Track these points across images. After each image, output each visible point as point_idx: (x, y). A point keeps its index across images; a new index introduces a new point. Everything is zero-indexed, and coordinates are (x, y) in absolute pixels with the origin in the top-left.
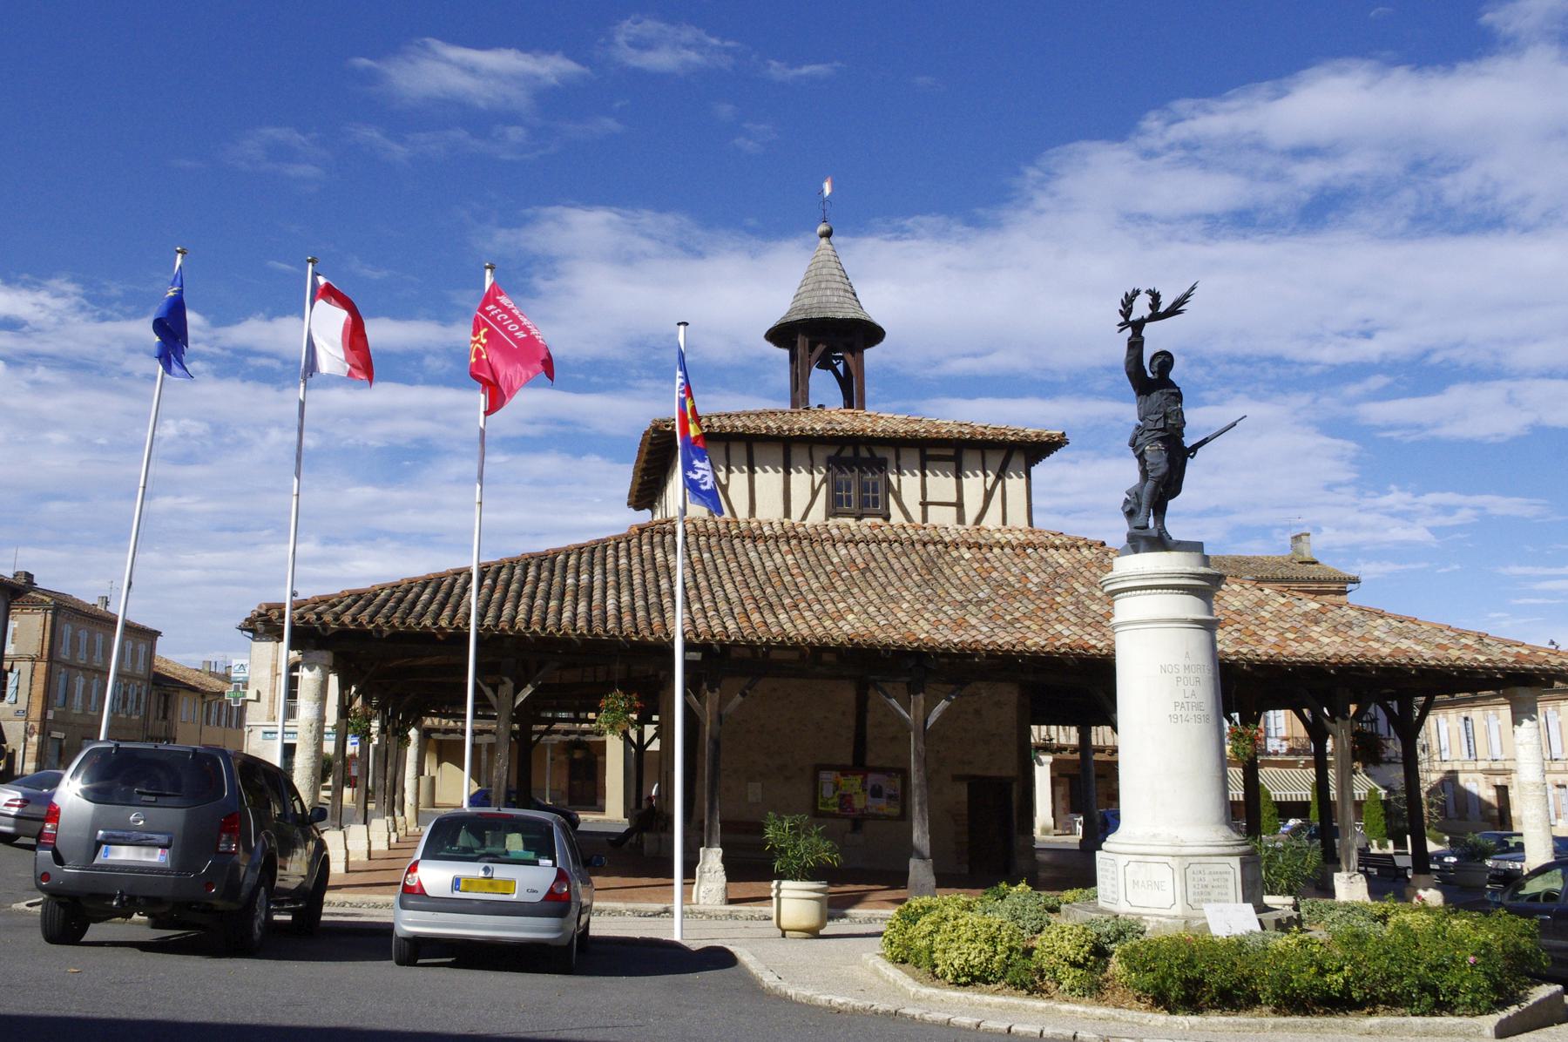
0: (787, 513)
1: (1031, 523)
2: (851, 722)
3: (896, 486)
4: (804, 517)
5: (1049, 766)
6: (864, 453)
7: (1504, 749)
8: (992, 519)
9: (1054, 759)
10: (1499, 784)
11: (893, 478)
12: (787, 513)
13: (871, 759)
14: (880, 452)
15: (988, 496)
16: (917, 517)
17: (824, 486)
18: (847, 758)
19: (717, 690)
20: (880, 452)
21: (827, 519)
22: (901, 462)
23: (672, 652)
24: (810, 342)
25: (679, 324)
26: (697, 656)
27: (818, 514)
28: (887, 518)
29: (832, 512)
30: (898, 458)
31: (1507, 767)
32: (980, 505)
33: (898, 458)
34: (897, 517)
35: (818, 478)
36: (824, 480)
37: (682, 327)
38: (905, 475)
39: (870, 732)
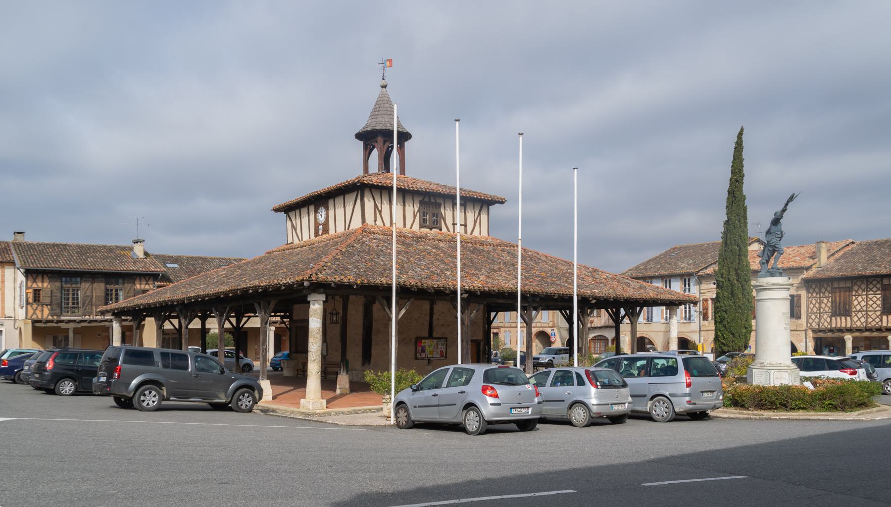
0: (405, 226)
1: (375, 224)
2: (428, 318)
3: (444, 216)
4: (411, 228)
5: (273, 332)
6: (433, 200)
7: (512, 317)
8: (476, 233)
9: (276, 328)
10: (495, 332)
11: (443, 211)
12: (405, 226)
13: (435, 335)
14: (438, 201)
15: (475, 222)
16: (451, 230)
17: (418, 213)
18: (426, 334)
19: (469, 308)
20: (438, 201)
21: (420, 229)
22: (446, 205)
23: (517, 296)
24: (384, 140)
25: (574, 169)
26: (466, 296)
27: (416, 227)
28: (441, 230)
29: (421, 227)
30: (444, 204)
31: (499, 325)
32: (473, 226)
33: (444, 204)
34: (444, 230)
35: (416, 209)
36: (419, 211)
37: (576, 170)
38: (384, 204)
39: (435, 323)
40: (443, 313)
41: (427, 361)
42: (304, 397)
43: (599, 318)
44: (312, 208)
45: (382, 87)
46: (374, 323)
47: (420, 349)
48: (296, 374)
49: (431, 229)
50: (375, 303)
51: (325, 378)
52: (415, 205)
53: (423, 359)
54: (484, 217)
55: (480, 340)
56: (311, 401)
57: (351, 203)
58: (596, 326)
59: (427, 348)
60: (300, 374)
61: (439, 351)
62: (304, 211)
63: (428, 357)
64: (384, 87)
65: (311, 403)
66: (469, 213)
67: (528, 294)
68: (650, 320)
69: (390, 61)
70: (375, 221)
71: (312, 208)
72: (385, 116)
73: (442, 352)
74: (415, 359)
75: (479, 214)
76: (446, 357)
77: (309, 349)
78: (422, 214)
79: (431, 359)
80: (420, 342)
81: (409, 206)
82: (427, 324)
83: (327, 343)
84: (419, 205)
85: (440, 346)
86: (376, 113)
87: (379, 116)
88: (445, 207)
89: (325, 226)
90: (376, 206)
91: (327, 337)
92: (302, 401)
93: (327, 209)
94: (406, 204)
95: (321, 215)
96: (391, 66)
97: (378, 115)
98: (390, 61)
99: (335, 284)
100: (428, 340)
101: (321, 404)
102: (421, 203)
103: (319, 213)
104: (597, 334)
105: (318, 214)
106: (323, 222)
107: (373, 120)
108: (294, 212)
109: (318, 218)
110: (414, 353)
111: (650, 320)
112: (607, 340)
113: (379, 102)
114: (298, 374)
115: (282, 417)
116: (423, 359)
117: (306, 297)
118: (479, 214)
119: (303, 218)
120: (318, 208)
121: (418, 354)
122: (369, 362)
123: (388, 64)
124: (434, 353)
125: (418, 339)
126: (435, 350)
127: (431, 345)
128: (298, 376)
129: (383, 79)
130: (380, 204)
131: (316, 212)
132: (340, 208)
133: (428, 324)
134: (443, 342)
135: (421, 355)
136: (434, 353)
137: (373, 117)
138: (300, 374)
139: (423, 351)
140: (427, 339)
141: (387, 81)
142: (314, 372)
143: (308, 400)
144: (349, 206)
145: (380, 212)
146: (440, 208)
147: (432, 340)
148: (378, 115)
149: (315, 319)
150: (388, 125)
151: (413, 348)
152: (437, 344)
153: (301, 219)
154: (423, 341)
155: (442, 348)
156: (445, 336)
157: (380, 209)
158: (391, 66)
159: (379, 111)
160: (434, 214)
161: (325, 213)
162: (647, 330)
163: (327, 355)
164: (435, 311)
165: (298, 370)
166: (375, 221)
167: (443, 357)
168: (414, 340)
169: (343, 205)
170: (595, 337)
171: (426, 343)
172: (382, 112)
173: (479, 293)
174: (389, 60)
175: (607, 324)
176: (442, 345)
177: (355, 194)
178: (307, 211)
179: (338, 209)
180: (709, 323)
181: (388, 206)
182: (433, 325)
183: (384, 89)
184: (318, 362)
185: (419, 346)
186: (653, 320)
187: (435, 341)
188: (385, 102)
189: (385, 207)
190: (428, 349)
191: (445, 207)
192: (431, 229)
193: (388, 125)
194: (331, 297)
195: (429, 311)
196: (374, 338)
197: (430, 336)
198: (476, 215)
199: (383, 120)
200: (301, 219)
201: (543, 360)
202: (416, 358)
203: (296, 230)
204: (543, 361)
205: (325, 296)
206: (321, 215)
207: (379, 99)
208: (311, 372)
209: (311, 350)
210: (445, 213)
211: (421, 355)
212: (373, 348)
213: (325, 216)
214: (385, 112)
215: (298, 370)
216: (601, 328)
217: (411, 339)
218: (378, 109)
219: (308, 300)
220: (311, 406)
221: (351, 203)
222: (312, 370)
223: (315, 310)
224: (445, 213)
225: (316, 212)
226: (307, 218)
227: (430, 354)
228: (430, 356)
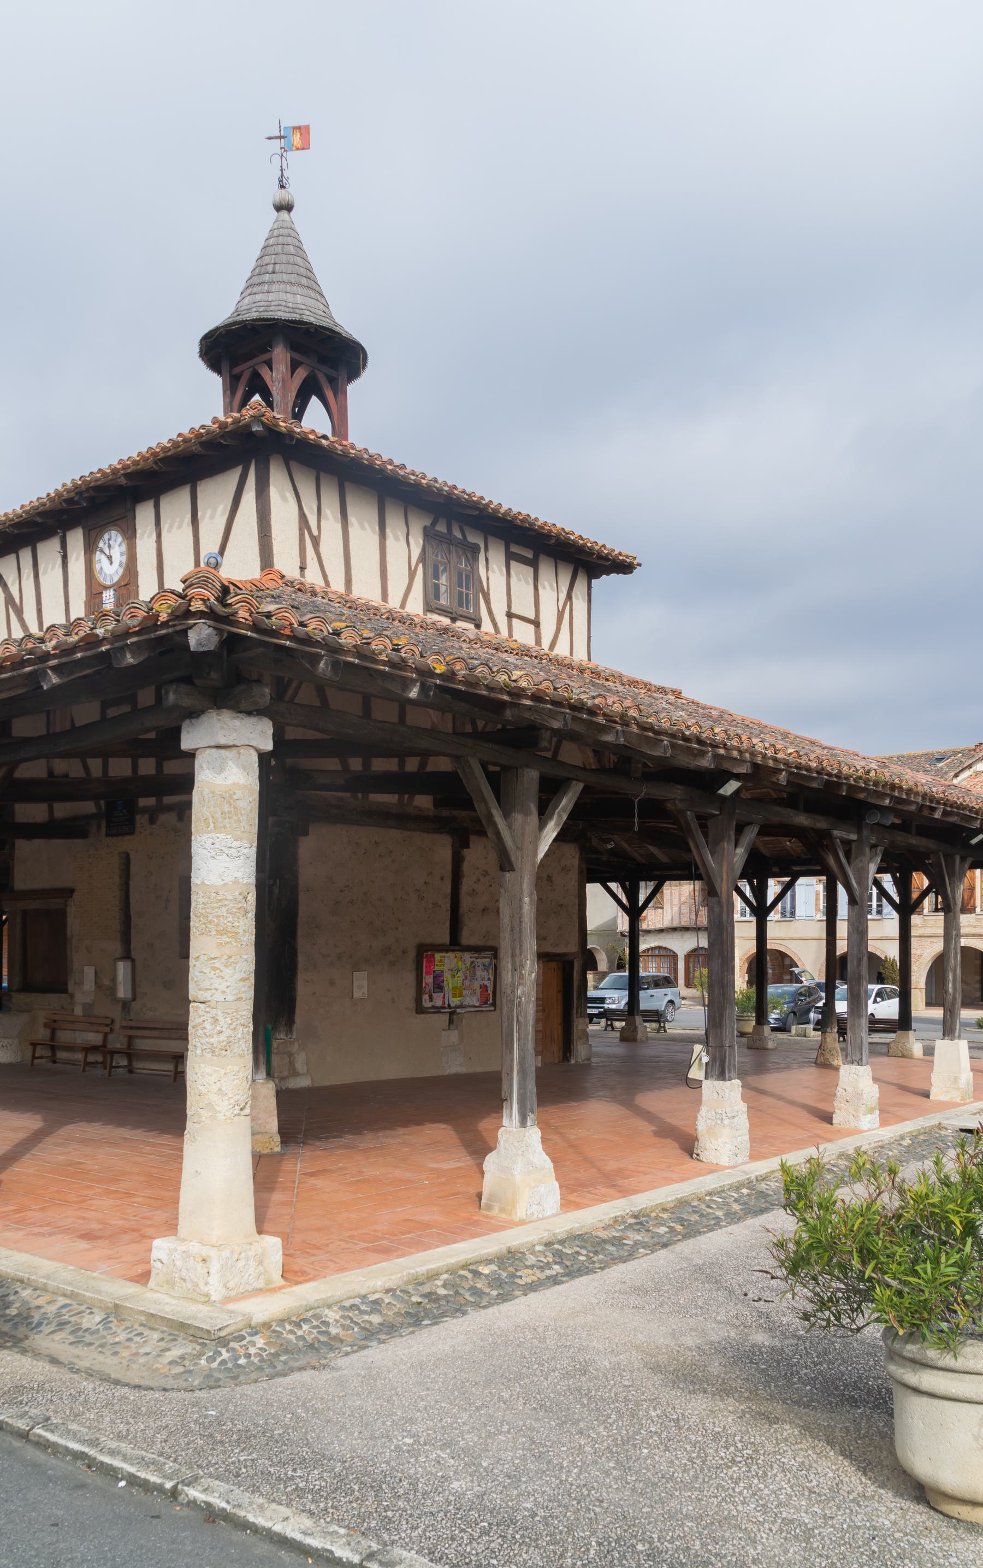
0: (385, 596)
2: (448, 888)
12: (385, 596)
13: (466, 939)
17: (421, 566)
28: (478, 626)
29: (429, 608)
30: (486, 550)
33: (486, 550)
34: (487, 626)
35: (416, 551)
36: (423, 558)
39: (466, 902)
40: (486, 874)
41: (446, 1017)
42: (171, 1227)
43: (659, 910)
44: (76, 539)
45: (279, 208)
46: (303, 899)
47: (428, 980)
48: (29, 1055)
49: (454, 620)
50: (306, 834)
51: (131, 1071)
52: (411, 540)
53: (437, 1010)
54: (579, 604)
55: (571, 954)
56: (213, 1253)
57: (220, 508)
58: (651, 927)
59: (447, 976)
60: (41, 1057)
61: (477, 985)
62: (49, 550)
63: (449, 1005)
64: (288, 207)
65: (215, 1267)
66: (544, 588)
67: (884, 795)
68: (788, 914)
69: (303, 131)
70: (302, 569)
71: (76, 539)
72: (295, 289)
73: (484, 988)
74: (417, 1013)
75: (569, 597)
76: (494, 1004)
77: (193, 992)
78: (430, 571)
79: (458, 1011)
80: (431, 960)
81: (397, 539)
82: (446, 905)
83: (133, 961)
84: (421, 542)
85: (479, 973)
86: (267, 278)
87: (275, 287)
88: (487, 560)
89: (124, 591)
90: (302, 516)
91: (133, 944)
92: (161, 1247)
93: (130, 535)
94: (388, 531)
95: (110, 558)
96: (305, 146)
97: (271, 283)
98: (303, 131)
99: (335, 665)
100: (450, 955)
101: (261, 1263)
102: (428, 534)
103: (102, 551)
104: (653, 945)
105: (98, 555)
106: (116, 579)
107: (258, 297)
108: (13, 556)
109: (97, 567)
110: (412, 992)
111: (788, 914)
112: (674, 956)
113: (271, 250)
114: (34, 1057)
115: (133, 1480)
116: (437, 1010)
117: (175, 734)
118: (569, 597)
119: (45, 572)
120: (99, 536)
121: (425, 997)
122: (290, 1023)
123: (297, 139)
124: (465, 992)
125: (424, 952)
126: (467, 983)
127: (458, 971)
128: (36, 1061)
129: (282, 187)
130: (315, 517)
131: (90, 548)
132: (180, 526)
133: (448, 906)
134: (487, 961)
135: (431, 999)
136: (465, 992)
137: (256, 289)
138: (41, 1057)
139: (439, 987)
140: (447, 951)
141: (294, 193)
142: (224, 1107)
143: (195, 1248)
144: (212, 517)
145: (316, 541)
146: (476, 559)
147: (459, 954)
148: (271, 283)
149: (224, 839)
150: (307, 313)
151: (410, 978)
152: (473, 966)
153: (36, 576)
154: (438, 956)
155: (483, 976)
156: (490, 943)
157: (315, 533)
158: (305, 146)
159: (274, 272)
160: (460, 575)
161: (124, 548)
162: (783, 936)
163: (134, 1000)
164: (466, 866)
165: (34, 1045)
166: (302, 569)
167: (486, 1003)
168: (412, 954)
169: (189, 516)
170: (652, 949)
171: (446, 962)
172: (285, 277)
173: (783, 778)
174: (299, 128)
175: (676, 924)
176: (486, 968)
177: (233, 477)
178: (59, 549)
179: (169, 531)
180: (925, 920)
181: (339, 527)
182: (461, 911)
183: (284, 214)
184: (241, 1056)
185: (428, 973)
186: (798, 912)
187: (467, 956)
188: (291, 249)
189: (331, 529)
190: (449, 983)
191: (487, 560)
192: (454, 620)
193: (307, 313)
194: (147, 816)
195: (449, 867)
196: (302, 944)
197: (455, 944)
198: (563, 596)
199: (290, 297)
200: (36, 576)
201: (613, 1003)
202: (420, 1010)
203: (19, 612)
204: (613, 1007)
205: (270, 731)
206: (110, 558)
207: (271, 241)
208: (210, 1106)
209: (202, 996)
210: (488, 579)
211: (431, 999)
212: (301, 978)
213: (124, 559)
214: (293, 278)
215: (34, 1045)
216: (661, 931)
217: (404, 952)
218: (270, 268)
219: (187, 743)
220: (214, 1279)
221: (220, 508)
222: (213, 1098)
223: (228, 797)
224: (488, 579)
225: (90, 548)
226: (59, 571)
227: (454, 996)
228: (455, 1001)
